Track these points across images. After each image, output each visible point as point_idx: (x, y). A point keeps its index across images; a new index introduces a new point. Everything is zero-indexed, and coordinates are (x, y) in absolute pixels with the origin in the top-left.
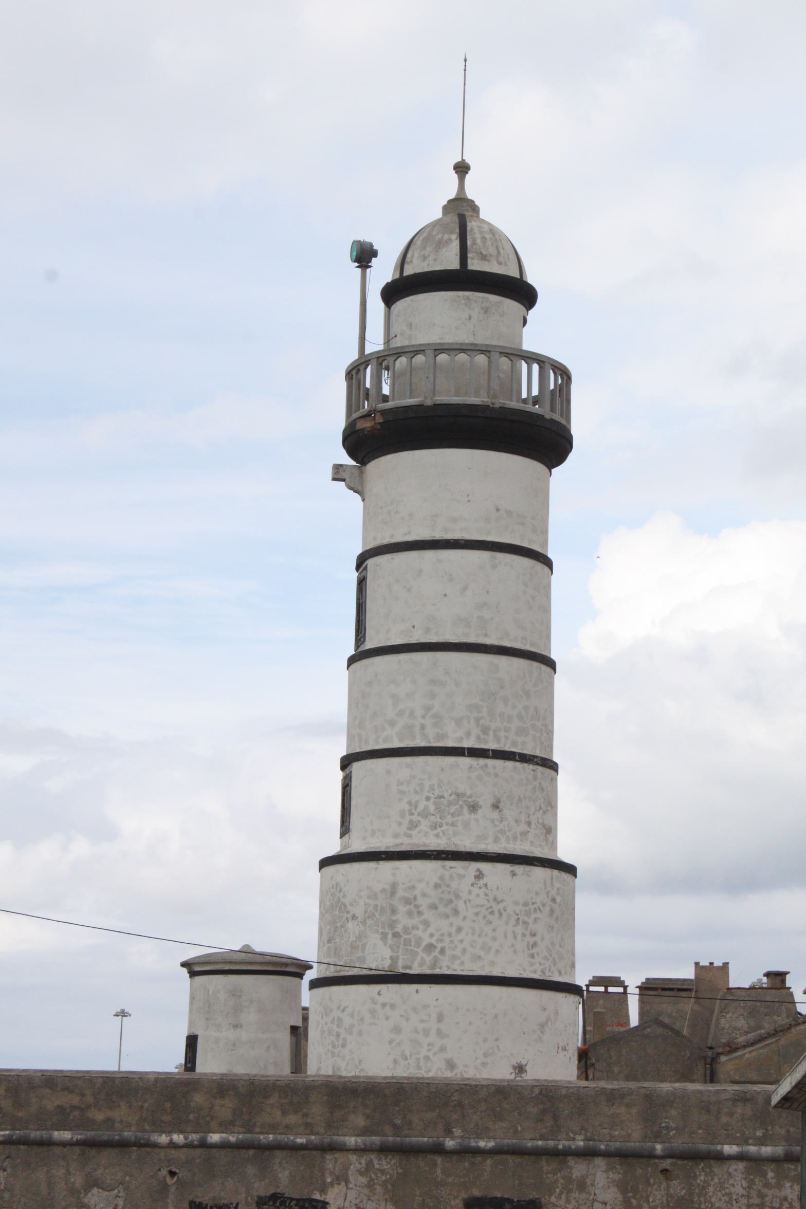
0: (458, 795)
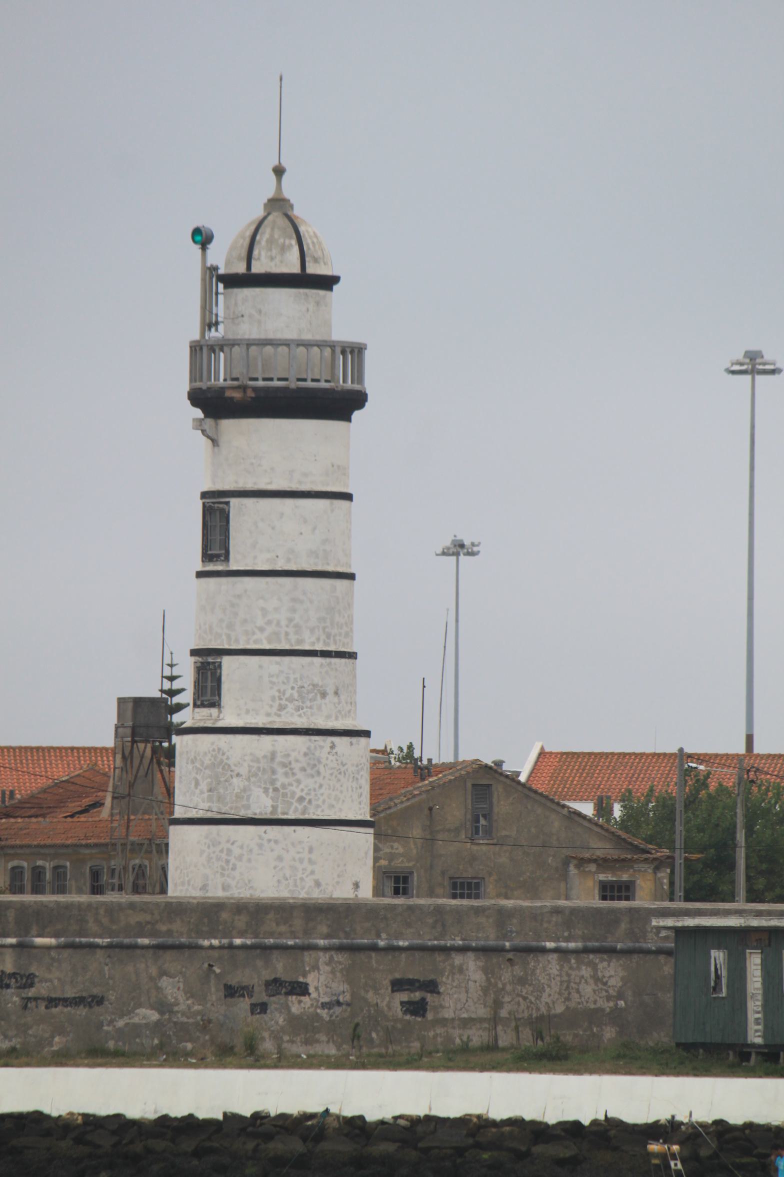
0: (314, 685)
